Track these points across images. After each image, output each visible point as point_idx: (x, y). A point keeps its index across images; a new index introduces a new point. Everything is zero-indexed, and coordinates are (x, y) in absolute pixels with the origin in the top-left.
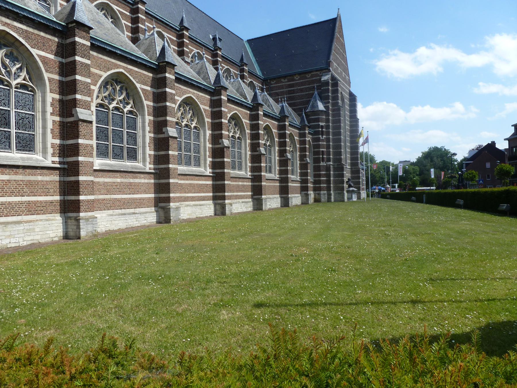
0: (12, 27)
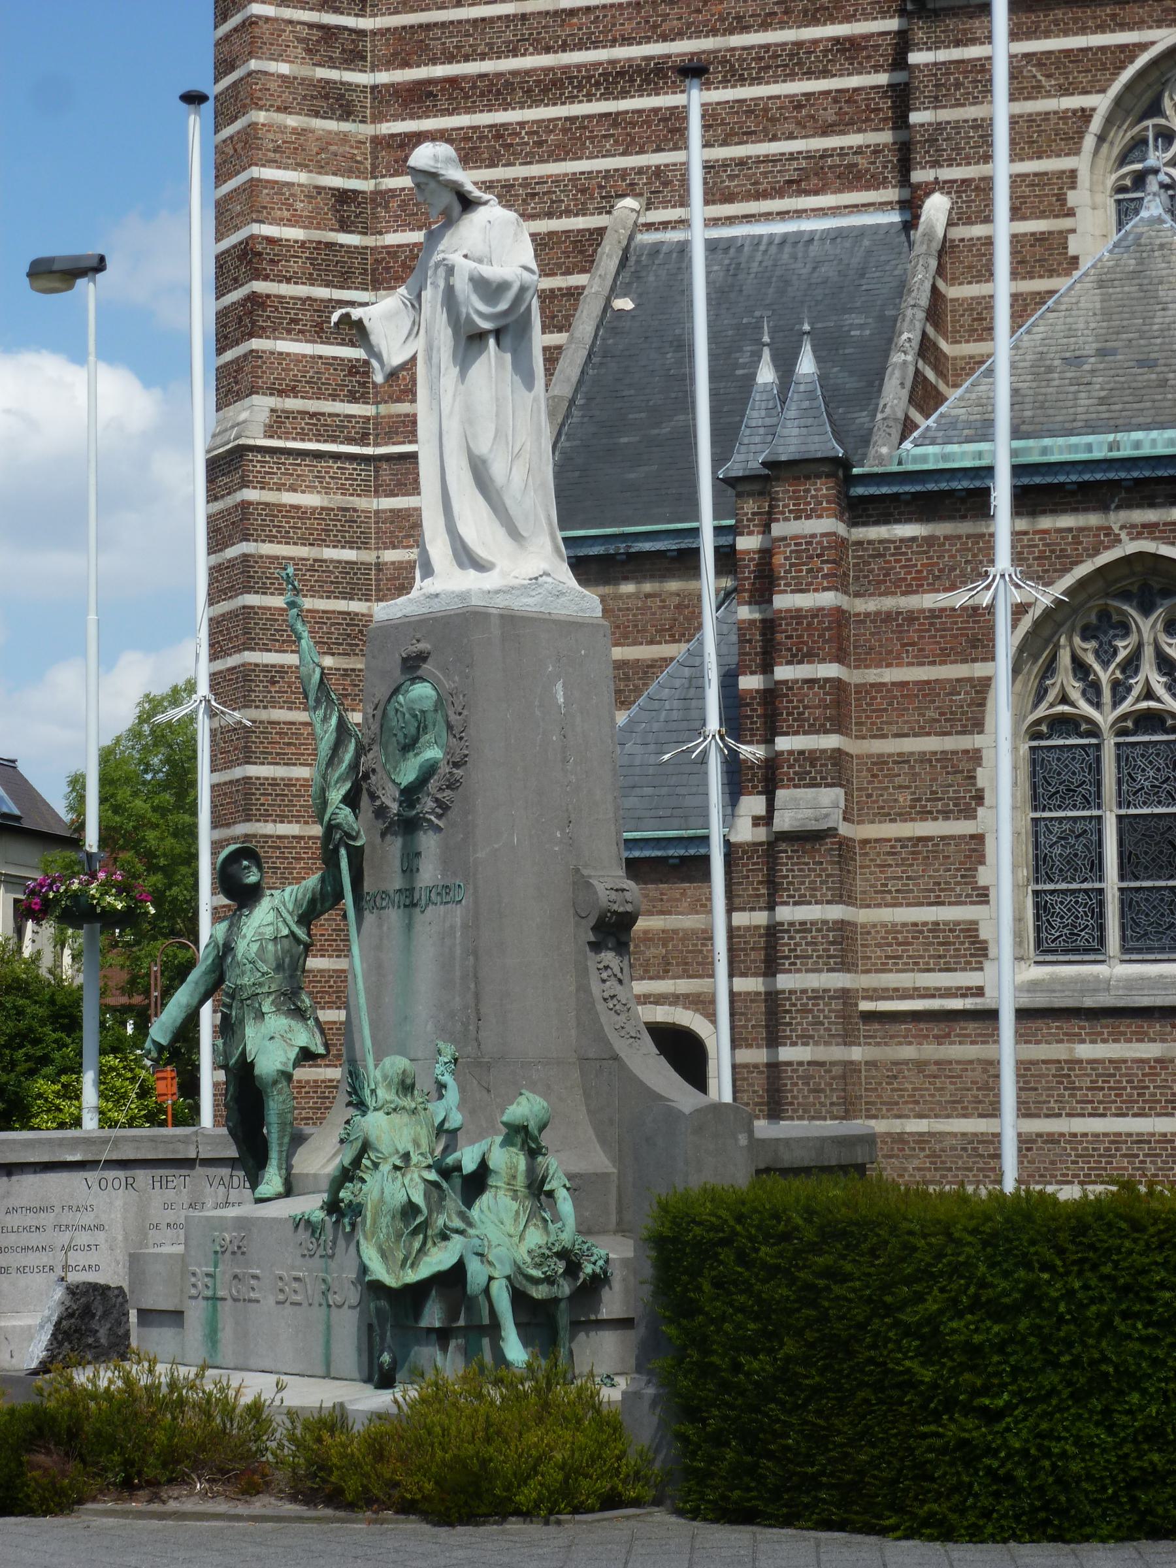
0: (1164, 531)
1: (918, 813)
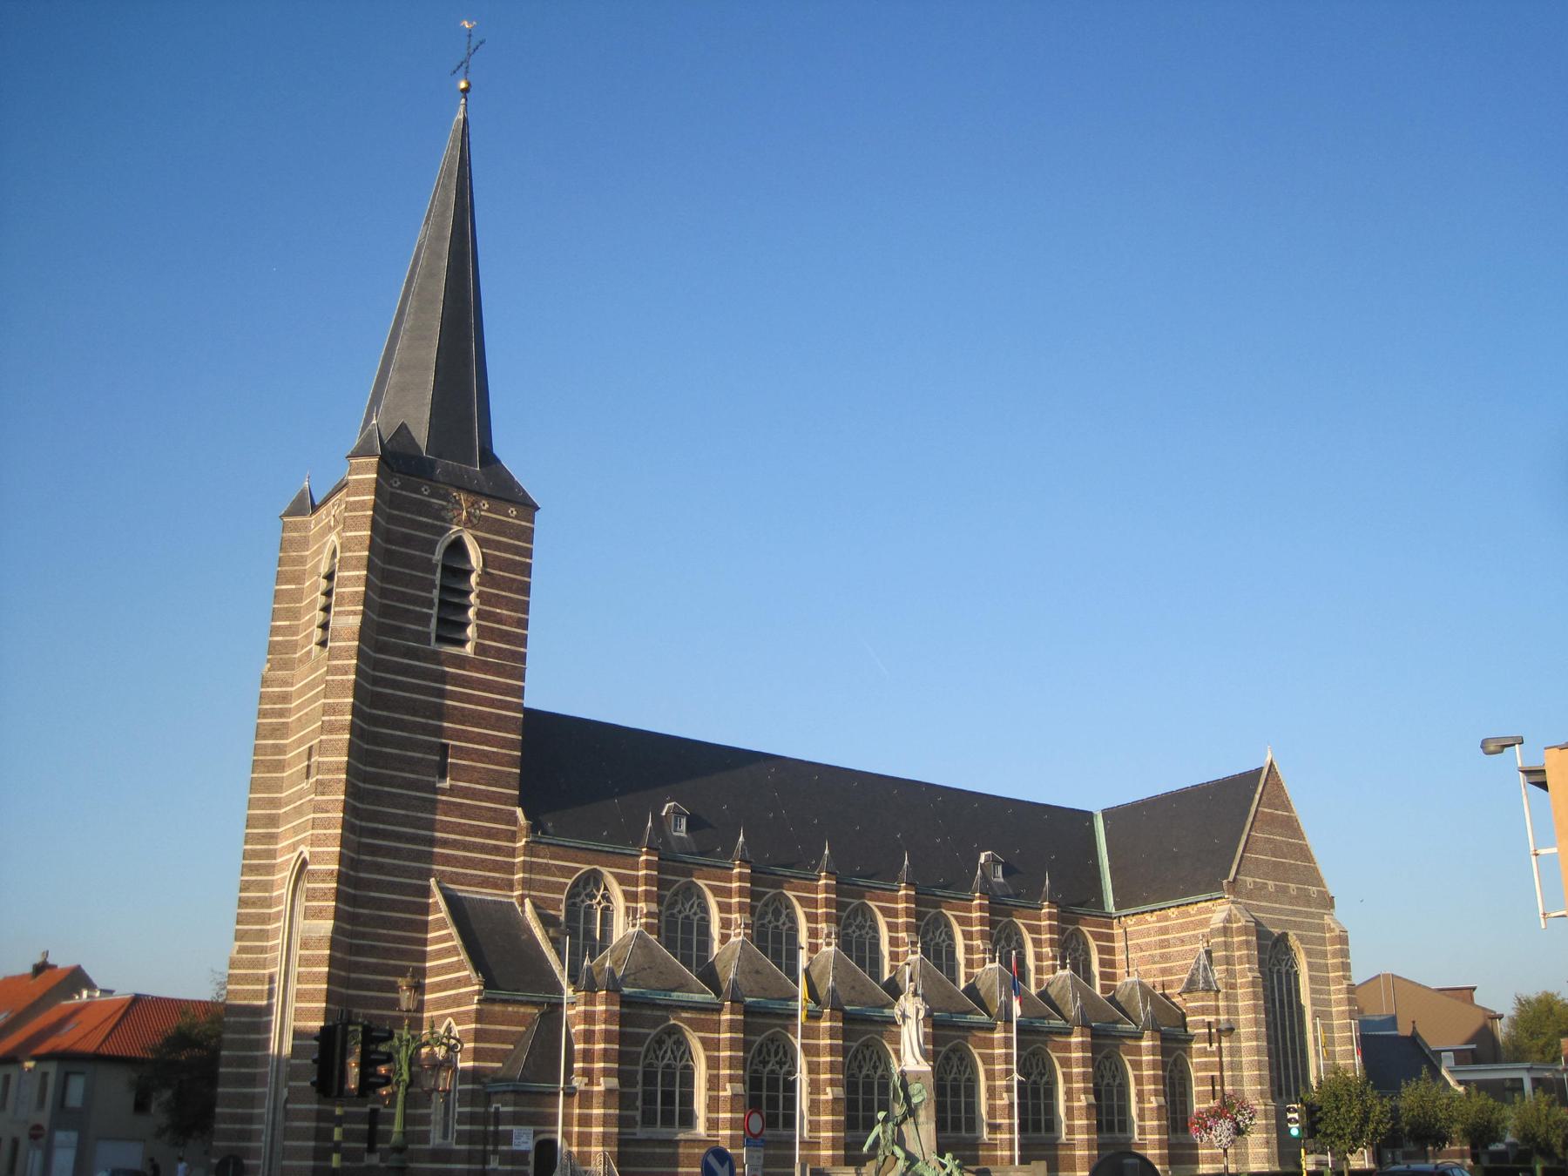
1: (310, 960)
